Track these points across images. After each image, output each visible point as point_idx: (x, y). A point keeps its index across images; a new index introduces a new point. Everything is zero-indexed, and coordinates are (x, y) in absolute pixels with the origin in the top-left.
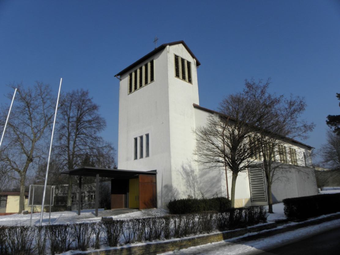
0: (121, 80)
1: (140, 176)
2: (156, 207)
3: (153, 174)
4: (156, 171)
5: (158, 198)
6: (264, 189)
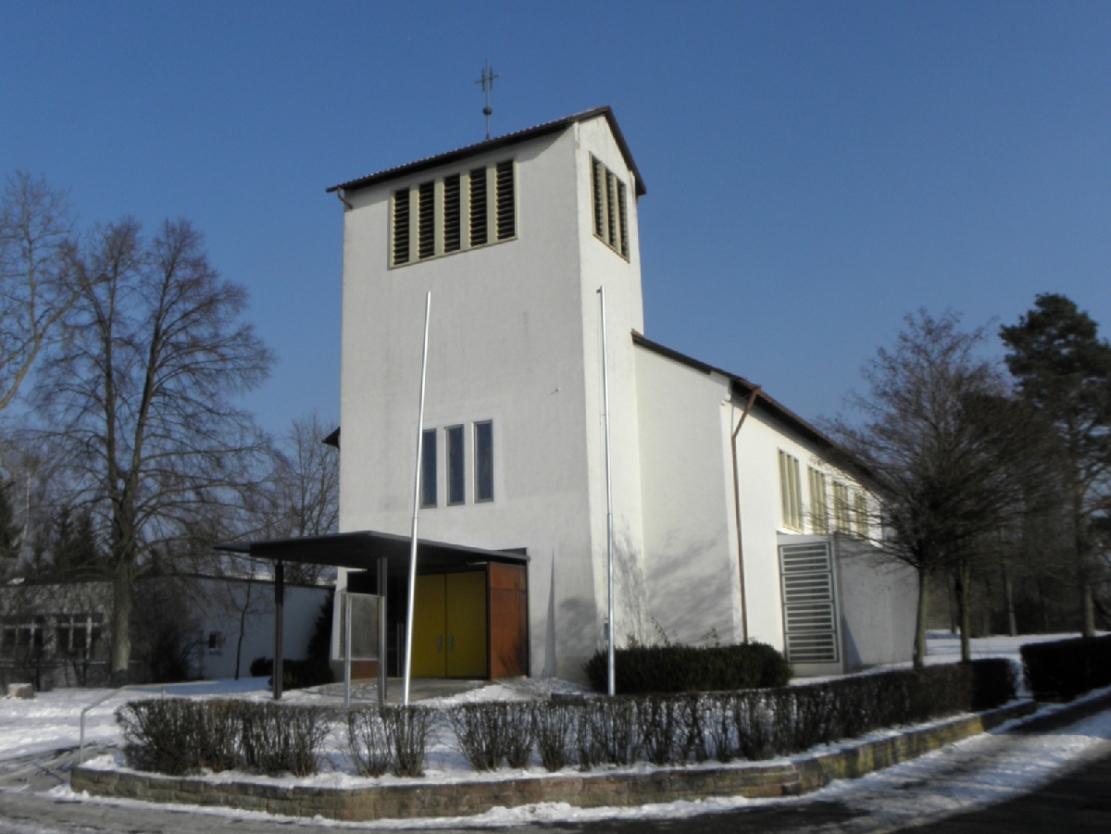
0: (350, 207)
1: (493, 566)
2: (527, 673)
3: (516, 561)
4: (523, 551)
5: (533, 642)
6: (832, 623)
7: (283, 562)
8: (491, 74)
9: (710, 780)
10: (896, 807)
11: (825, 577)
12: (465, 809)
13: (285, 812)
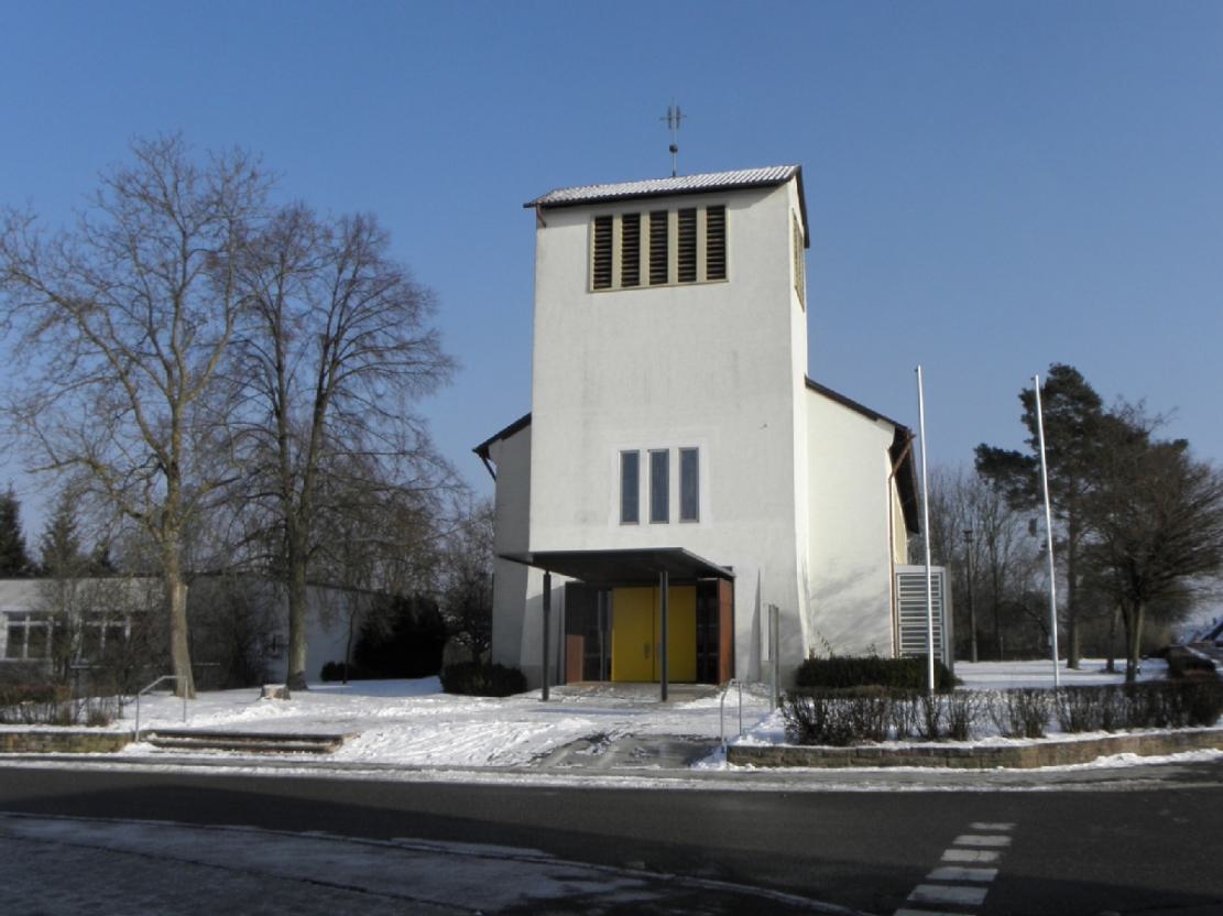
0: (545, 225)
5: (738, 650)
7: (550, 573)
8: (678, 113)
9: (1200, 738)
10: (551, 855)
11: (902, 595)
12: (1082, 758)
13: (965, 767)
